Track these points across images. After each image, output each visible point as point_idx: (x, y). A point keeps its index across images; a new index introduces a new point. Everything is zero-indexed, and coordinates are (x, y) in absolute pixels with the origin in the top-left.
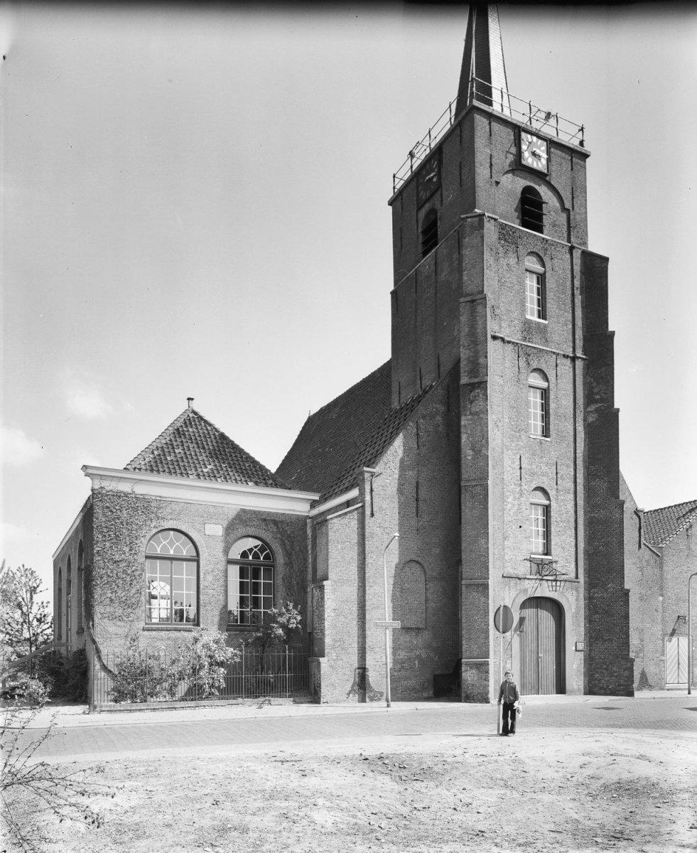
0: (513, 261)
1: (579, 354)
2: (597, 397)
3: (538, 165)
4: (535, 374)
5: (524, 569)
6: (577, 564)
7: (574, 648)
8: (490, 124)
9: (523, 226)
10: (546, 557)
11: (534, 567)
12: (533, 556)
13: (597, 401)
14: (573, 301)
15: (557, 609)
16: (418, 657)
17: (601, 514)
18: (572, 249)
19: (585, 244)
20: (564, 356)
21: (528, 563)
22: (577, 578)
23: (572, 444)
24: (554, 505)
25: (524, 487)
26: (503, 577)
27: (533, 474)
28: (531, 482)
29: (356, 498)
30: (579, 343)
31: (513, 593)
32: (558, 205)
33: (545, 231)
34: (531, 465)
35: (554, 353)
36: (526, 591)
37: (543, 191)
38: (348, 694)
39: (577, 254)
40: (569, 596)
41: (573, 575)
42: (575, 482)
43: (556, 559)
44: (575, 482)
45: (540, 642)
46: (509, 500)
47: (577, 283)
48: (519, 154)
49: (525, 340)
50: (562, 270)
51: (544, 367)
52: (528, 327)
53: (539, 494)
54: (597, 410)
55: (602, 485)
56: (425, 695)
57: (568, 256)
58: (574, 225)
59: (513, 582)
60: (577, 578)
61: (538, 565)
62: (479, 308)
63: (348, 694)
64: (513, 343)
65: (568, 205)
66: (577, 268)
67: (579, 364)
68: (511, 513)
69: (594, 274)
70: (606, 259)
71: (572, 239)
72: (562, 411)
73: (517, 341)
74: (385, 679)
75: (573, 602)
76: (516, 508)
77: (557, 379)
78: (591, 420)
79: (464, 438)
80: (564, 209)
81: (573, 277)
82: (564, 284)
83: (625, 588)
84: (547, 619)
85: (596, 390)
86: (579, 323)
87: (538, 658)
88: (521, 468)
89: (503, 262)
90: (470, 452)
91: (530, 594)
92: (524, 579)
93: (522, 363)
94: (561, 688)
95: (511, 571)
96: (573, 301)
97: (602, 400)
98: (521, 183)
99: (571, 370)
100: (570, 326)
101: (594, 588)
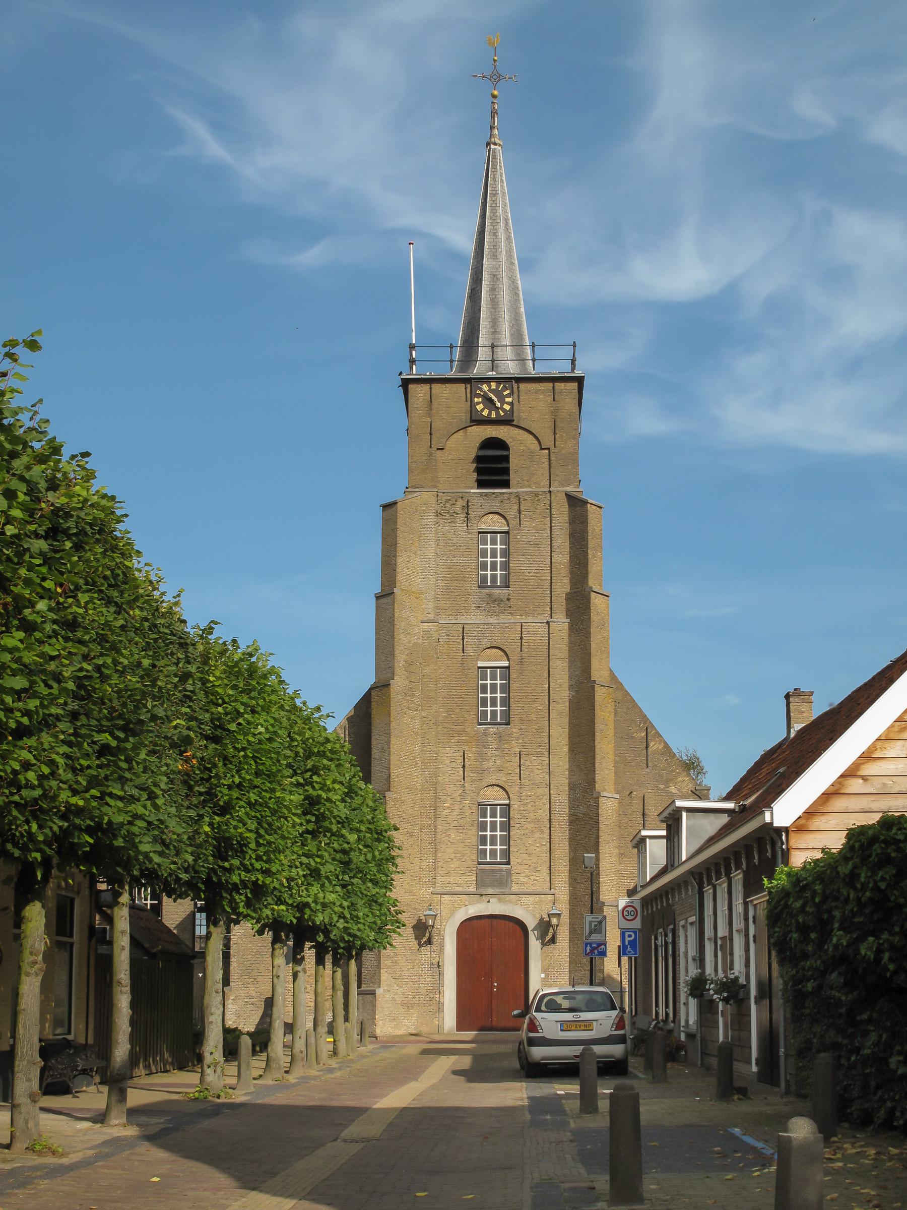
24: (515, 806)
65: (547, 441)
76: (457, 811)
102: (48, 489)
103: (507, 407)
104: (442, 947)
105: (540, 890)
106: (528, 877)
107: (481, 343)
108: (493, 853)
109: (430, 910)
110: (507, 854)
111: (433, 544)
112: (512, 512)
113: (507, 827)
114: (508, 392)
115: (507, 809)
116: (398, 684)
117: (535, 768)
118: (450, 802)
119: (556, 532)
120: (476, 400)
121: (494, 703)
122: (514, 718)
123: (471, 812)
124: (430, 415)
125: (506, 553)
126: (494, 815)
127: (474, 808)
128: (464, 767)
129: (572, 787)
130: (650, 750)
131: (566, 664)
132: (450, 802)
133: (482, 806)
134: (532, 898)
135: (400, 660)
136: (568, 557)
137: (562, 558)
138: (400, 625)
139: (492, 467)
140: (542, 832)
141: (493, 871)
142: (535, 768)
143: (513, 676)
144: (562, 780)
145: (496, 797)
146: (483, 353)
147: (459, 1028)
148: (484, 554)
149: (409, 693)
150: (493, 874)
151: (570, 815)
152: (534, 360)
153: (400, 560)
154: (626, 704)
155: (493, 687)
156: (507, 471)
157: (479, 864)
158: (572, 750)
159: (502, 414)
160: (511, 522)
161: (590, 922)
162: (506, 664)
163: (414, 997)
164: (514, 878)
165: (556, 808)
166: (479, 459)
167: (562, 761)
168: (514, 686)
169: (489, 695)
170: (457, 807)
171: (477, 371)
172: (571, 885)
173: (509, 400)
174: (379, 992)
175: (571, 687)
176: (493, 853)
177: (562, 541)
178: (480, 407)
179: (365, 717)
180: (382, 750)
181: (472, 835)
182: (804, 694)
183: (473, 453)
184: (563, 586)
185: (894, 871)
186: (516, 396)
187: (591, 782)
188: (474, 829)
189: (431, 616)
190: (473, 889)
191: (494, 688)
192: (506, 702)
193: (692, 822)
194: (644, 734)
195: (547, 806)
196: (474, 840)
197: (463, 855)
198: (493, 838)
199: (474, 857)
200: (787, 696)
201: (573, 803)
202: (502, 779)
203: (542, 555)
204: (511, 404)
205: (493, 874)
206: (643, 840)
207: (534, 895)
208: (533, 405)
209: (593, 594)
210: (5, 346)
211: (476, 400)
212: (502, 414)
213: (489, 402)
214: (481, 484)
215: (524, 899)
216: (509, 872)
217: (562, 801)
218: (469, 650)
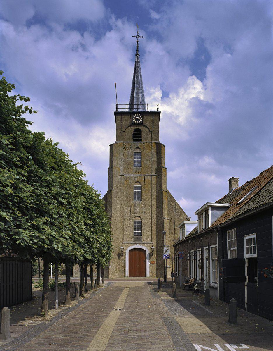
3: (139, 122)
9: (134, 141)
24: (143, 221)
37: (141, 128)
65: (151, 130)
103: (141, 120)
104: (125, 256)
105: (149, 242)
106: (146, 239)
107: (134, 103)
108: (138, 233)
109: (122, 247)
110: (141, 233)
111: (122, 155)
112: (142, 148)
113: (141, 227)
114: (141, 116)
115: (141, 222)
116: (114, 190)
117: (148, 211)
118: (127, 220)
119: (153, 152)
120: (133, 118)
121: (138, 196)
122: (143, 200)
123: (132, 223)
124: (122, 123)
125: (141, 158)
126: (138, 224)
127: (133, 222)
128: (130, 212)
129: (157, 217)
130: (176, 208)
131: (156, 186)
132: (127, 220)
133: (135, 222)
134: (147, 244)
135: (114, 184)
136: (156, 159)
137: (155, 159)
138: (114, 175)
140: (150, 228)
141: (138, 237)
142: (148, 211)
144: (154, 215)
145: (138, 219)
146: (135, 106)
147: (129, 276)
148: (135, 158)
149: (117, 193)
150: (138, 238)
151: (157, 224)
152: (148, 108)
153: (114, 159)
155: (138, 192)
156: (141, 137)
157: (134, 236)
158: (157, 208)
159: (140, 122)
160: (142, 150)
161: (165, 249)
162: (140, 186)
163: (118, 268)
164: (143, 239)
166: (134, 134)
167: (154, 210)
168: (143, 191)
169: (136, 197)
170: (129, 221)
171: (135, 110)
172: (157, 241)
173: (142, 118)
174: (110, 267)
175: (157, 192)
176: (138, 233)
177: (155, 155)
179: (106, 197)
180: (110, 207)
181: (133, 228)
182: (236, 178)
183: (132, 133)
184: (155, 167)
186: (143, 117)
187: (162, 215)
188: (133, 227)
189: (122, 174)
190: (132, 242)
192: (141, 195)
193: (213, 211)
194: (174, 204)
195: (151, 221)
196: (133, 230)
197: (130, 233)
199: (133, 234)
200: (230, 180)
201: (157, 220)
202: (139, 215)
203: (150, 156)
204: (142, 119)
205: (138, 238)
206: (184, 224)
207: (147, 245)
210: (3, 77)
211: (133, 118)
212: (140, 122)
213: (137, 120)
214: (134, 140)
215: (145, 244)
216: (141, 238)
217: (155, 219)
218: (132, 182)
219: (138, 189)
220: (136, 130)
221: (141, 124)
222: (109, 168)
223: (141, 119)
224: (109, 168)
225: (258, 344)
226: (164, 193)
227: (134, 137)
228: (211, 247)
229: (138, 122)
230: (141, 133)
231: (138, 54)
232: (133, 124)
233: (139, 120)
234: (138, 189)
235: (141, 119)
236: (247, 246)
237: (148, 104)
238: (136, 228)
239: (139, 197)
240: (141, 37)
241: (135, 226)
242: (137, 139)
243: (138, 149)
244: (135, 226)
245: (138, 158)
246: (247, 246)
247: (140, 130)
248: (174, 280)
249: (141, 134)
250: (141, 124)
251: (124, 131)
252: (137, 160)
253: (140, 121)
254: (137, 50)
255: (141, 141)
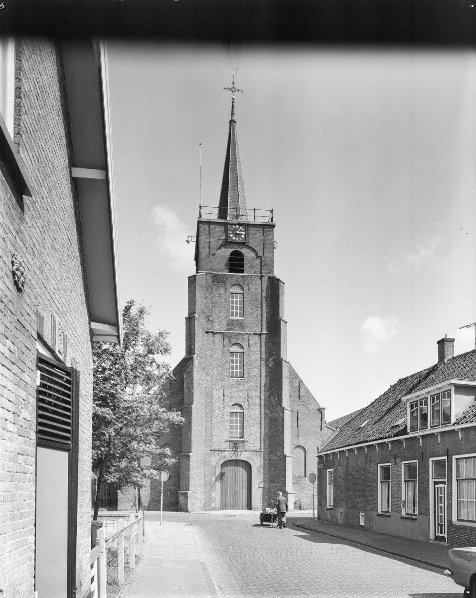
0: (222, 291)
1: (265, 331)
2: (274, 353)
3: (239, 239)
4: (235, 347)
5: (225, 446)
6: (261, 442)
7: (258, 486)
8: (209, 226)
9: (231, 272)
10: (242, 439)
11: (232, 445)
12: (231, 439)
13: (273, 356)
14: (262, 304)
15: (247, 466)
16: (170, 490)
17: (274, 415)
18: (261, 277)
19: (272, 272)
20: (254, 334)
21: (228, 443)
22: (261, 449)
23: (259, 380)
24: (246, 412)
25: (226, 404)
26: (211, 450)
27: (232, 397)
28: (231, 401)
29: (436, 365)
30: (265, 325)
31: (217, 458)
32: (254, 255)
33: (245, 271)
34: (231, 393)
35: (247, 334)
36: (225, 457)
37: (244, 251)
38: (132, 507)
39: (265, 279)
40: (255, 458)
41: (258, 448)
42: (260, 399)
43: (247, 440)
44: (260, 399)
45: (236, 482)
46: (216, 412)
47: (264, 294)
48: (227, 236)
49: (228, 330)
50: (257, 288)
51: (240, 342)
52: (231, 324)
53: (237, 407)
54: (273, 360)
55: (274, 400)
56: (173, 508)
57: (259, 281)
58: (266, 263)
59: (217, 453)
60: (261, 449)
61: (235, 443)
62: (192, 321)
63: (132, 507)
64: (220, 333)
65: (260, 254)
66: (265, 287)
67: (264, 337)
68: (218, 418)
69: (274, 288)
70: (189, 278)
71: (262, 272)
72: (252, 363)
73: (225, 332)
74: (377, 437)
75: (257, 464)
76: (220, 415)
77: (249, 347)
78: (271, 365)
79: (185, 384)
80: (258, 257)
81: (262, 292)
82: (256, 297)
83: (99, 508)
84: (242, 472)
85: (273, 350)
86: (265, 315)
87: (235, 491)
88: (224, 395)
89: (216, 293)
90: (187, 391)
91: (228, 458)
92: (224, 451)
93: (226, 342)
94: (249, 507)
95: (215, 447)
96: (262, 304)
97: (275, 355)
98: (228, 251)
99: (259, 341)
100: (260, 318)
101: (271, 454)
102: (115, 429)
139: (236, 263)
143: (245, 356)
154: (294, 376)
156: (242, 266)
162: (241, 351)
165: (263, 286)
166: (230, 259)
168: (246, 361)
171: (229, 219)
178: (231, 235)
185: (339, 522)
191: (237, 361)
196: (229, 427)
198: (236, 426)
202: (240, 401)
208: (255, 238)
209: (281, 321)
219: (237, 298)
220: (233, 253)
221: (243, 244)
222: (186, 318)
223: (243, 234)
224: (186, 318)
225: (350, 581)
226: (284, 363)
227: (231, 265)
228: (454, 457)
229: (237, 239)
230: (243, 265)
231: (234, 121)
232: (227, 243)
233: (241, 234)
234: (236, 357)
235: (243, 234)
236: (160, 510)
237: (255, 209)
238: (234, 370)
239: (239, 300)
240: (238, 91)
241: (232, 362)
242: (235, 269)
243: (237, 287)
244: (232, 362)
245: (237, 303)
246: (160, 510)
247: (240, 254)
248: (316, 516)
249: (242, 260)
250: (243, 244)
251: (213, 255)
252: (237, 304)
253: (242, 237)
254: (232, 114)
255: (243, 272)
